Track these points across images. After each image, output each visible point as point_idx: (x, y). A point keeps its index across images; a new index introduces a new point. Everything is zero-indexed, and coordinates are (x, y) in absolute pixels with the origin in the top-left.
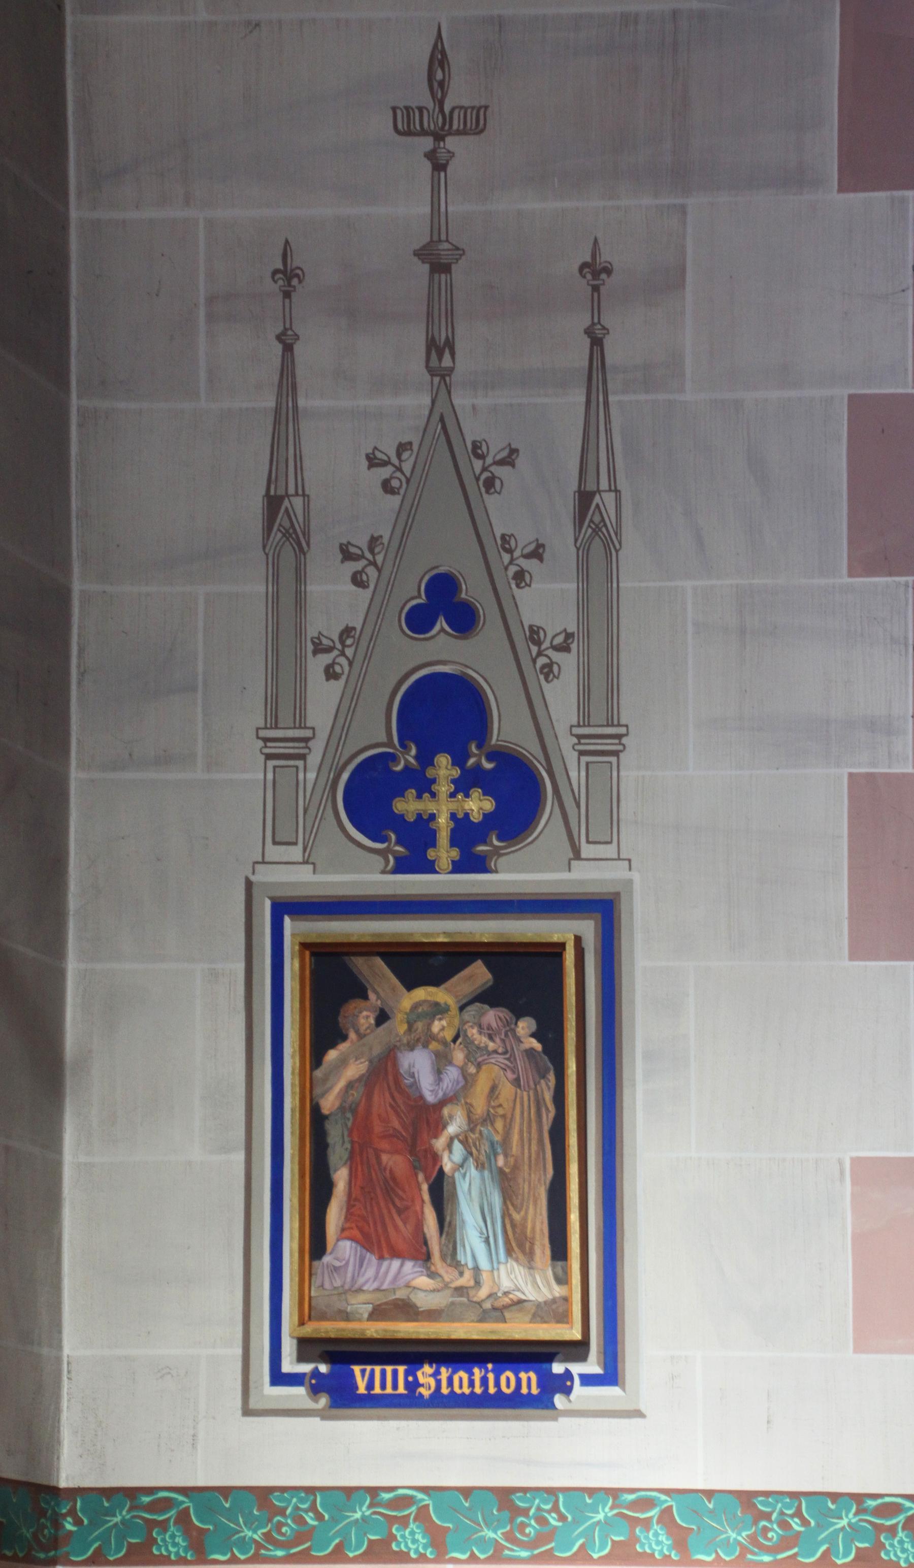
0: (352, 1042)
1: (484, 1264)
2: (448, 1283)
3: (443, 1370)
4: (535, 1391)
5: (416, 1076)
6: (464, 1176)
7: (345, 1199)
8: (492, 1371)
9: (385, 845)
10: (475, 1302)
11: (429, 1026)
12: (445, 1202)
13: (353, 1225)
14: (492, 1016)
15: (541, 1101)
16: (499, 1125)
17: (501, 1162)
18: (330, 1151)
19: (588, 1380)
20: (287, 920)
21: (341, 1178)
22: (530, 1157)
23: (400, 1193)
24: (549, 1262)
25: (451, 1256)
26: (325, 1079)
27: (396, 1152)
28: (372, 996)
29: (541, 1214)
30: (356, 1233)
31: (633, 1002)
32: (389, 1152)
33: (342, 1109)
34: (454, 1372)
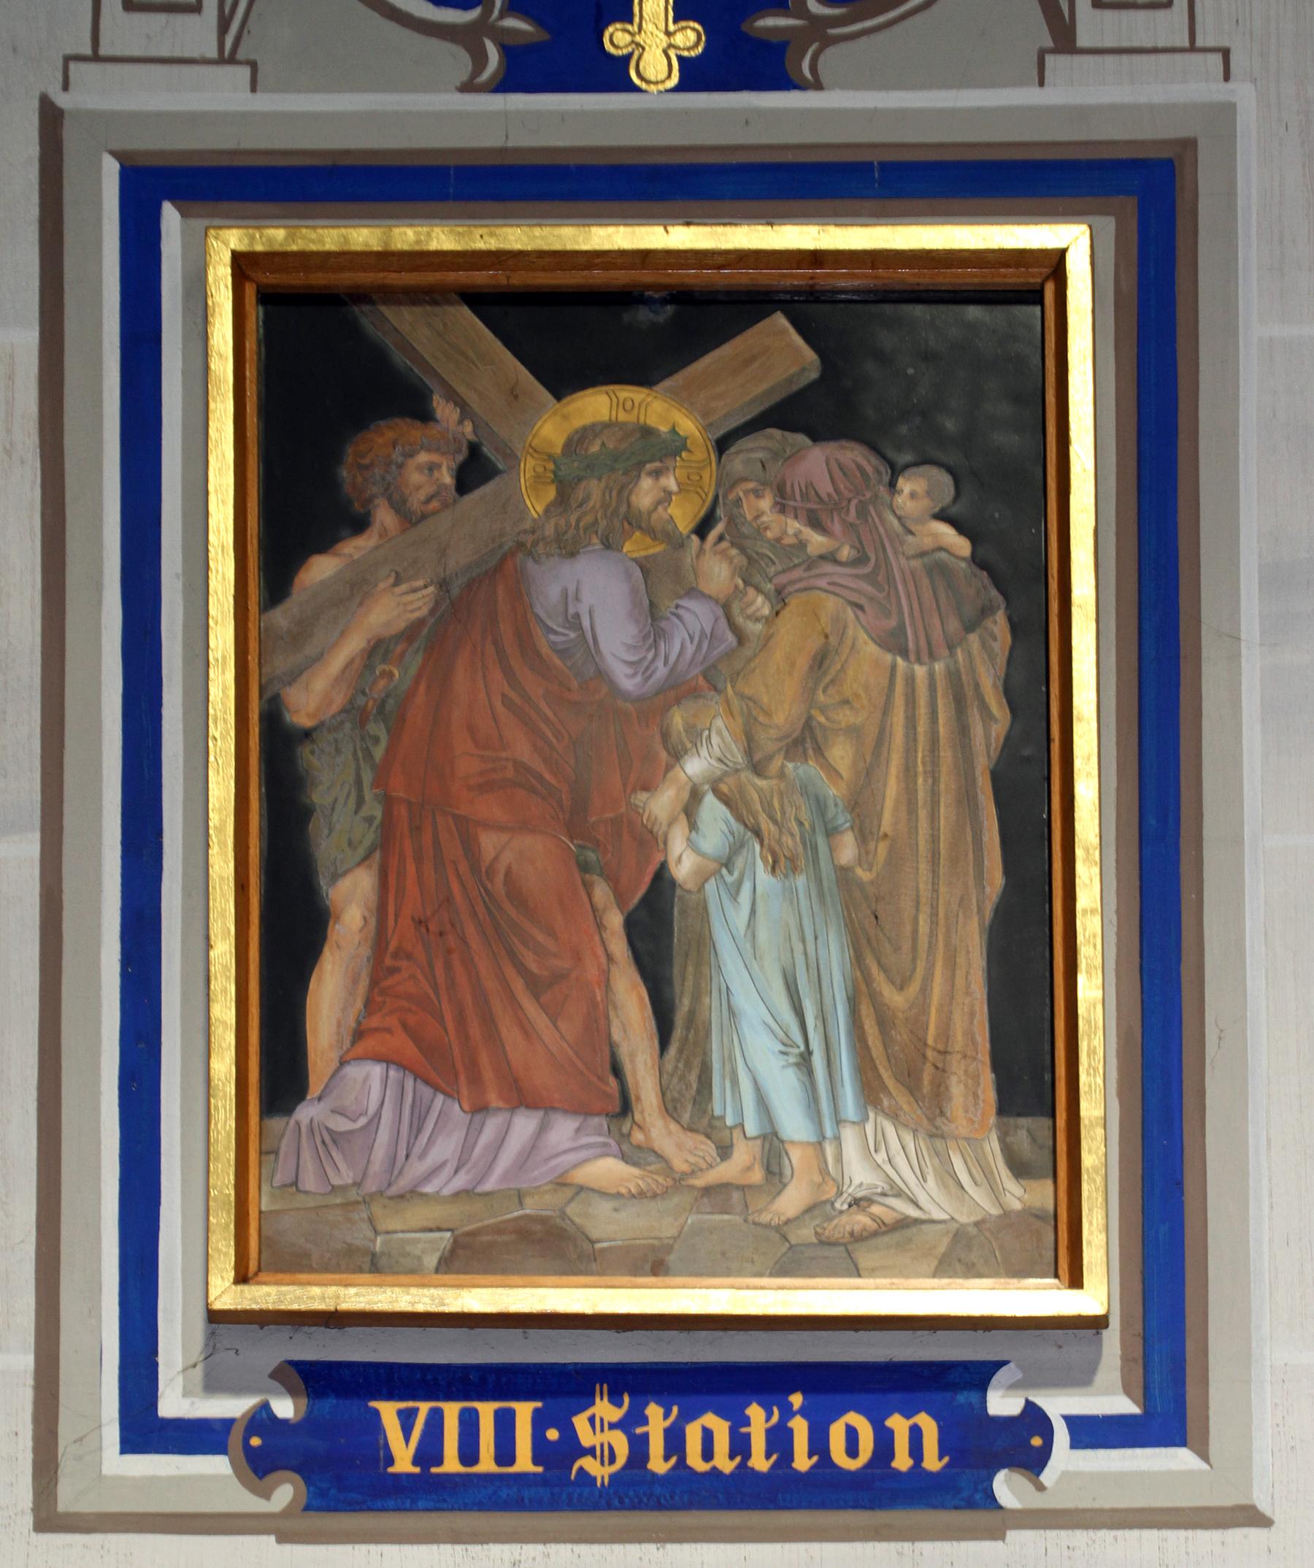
0: (383, 533)
1: (794, 1125)
2: (684, 1175)
3: (654, 1411)
4: (932, 1462)
5: (586, 623)
6: (735, 892)
7: (366, 951)
8: (803, 1412)
9: (474, 14)
10: (767, 1226)
11: (624, 491)
12: (677, 961)
13: (393, 1022)
14: (818, 463)
15: (969, 693)
16: (841, 754)
17: (848, 850)
18: (317, 827)
19: (1089, 1432)
20: (170, 215)
21: (351, 899)
22: (934, 839)
23: (541, 937)
24: (992, 1119)
25: (692, 1099)
26: (299, 635)
27: (525, 827)
28: (444, 410)
29: (968, 993)
30: (400, 1042)
31: (1233, 432)
32: (501, 828)
33: (356, 714)
34: (689, 1415)
